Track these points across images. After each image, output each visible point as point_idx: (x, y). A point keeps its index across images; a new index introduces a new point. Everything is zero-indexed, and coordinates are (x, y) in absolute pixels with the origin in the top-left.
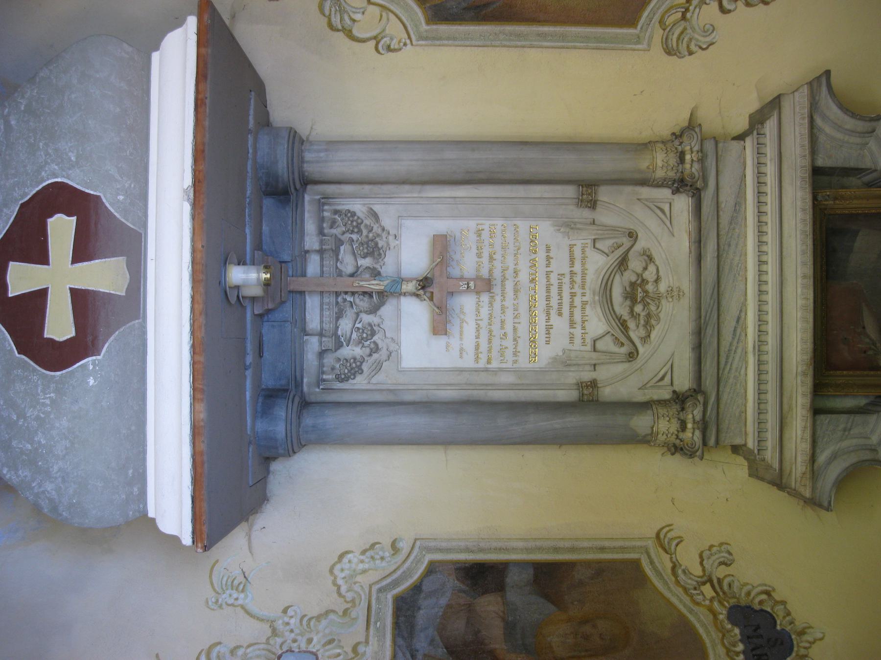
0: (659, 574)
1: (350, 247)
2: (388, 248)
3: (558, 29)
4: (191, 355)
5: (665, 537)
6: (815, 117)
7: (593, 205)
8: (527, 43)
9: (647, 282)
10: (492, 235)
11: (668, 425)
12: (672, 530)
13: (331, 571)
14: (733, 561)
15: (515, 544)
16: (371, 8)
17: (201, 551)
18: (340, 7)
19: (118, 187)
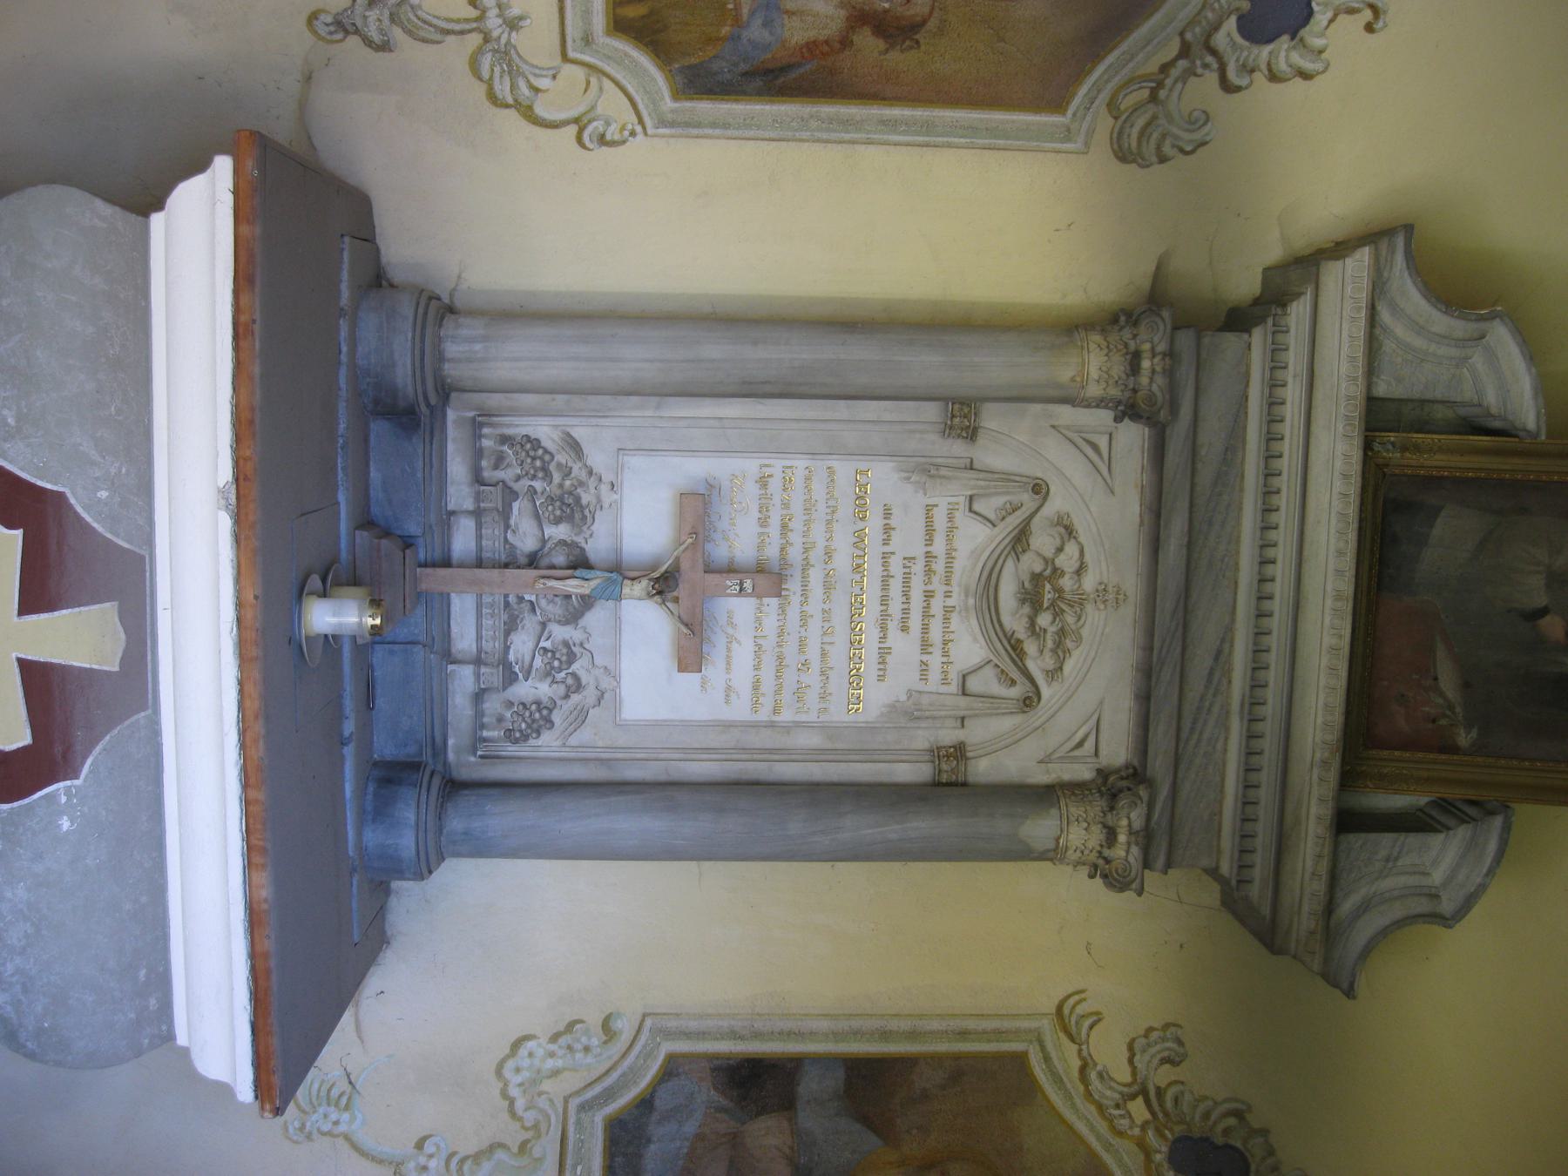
0: (1058, 1080)
1: (529, 505)
2: (598, 507)
3: (920, 113)
4: (241, 783)
5: (1071, 1013)
6: (1379, 308)
7: (971, 434)
8: (860, 136)
9: (1063, 573)
10: (786, 485)
11: (1085, 835)
12: (1085, 1000)
13: (499, 1071)
14: (1185, 1056)
15: (815, 1025)
16: (569, 69)
17: (271, 1116)
18: (509, 65)
19: (97, 475)
